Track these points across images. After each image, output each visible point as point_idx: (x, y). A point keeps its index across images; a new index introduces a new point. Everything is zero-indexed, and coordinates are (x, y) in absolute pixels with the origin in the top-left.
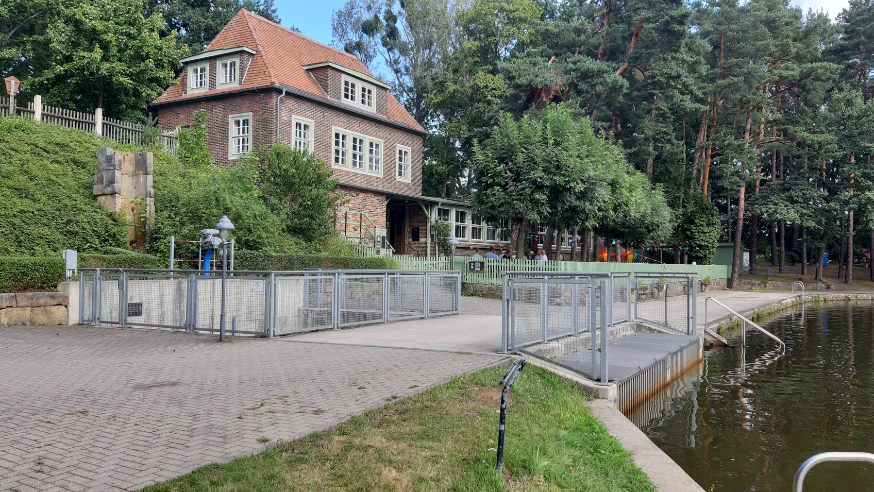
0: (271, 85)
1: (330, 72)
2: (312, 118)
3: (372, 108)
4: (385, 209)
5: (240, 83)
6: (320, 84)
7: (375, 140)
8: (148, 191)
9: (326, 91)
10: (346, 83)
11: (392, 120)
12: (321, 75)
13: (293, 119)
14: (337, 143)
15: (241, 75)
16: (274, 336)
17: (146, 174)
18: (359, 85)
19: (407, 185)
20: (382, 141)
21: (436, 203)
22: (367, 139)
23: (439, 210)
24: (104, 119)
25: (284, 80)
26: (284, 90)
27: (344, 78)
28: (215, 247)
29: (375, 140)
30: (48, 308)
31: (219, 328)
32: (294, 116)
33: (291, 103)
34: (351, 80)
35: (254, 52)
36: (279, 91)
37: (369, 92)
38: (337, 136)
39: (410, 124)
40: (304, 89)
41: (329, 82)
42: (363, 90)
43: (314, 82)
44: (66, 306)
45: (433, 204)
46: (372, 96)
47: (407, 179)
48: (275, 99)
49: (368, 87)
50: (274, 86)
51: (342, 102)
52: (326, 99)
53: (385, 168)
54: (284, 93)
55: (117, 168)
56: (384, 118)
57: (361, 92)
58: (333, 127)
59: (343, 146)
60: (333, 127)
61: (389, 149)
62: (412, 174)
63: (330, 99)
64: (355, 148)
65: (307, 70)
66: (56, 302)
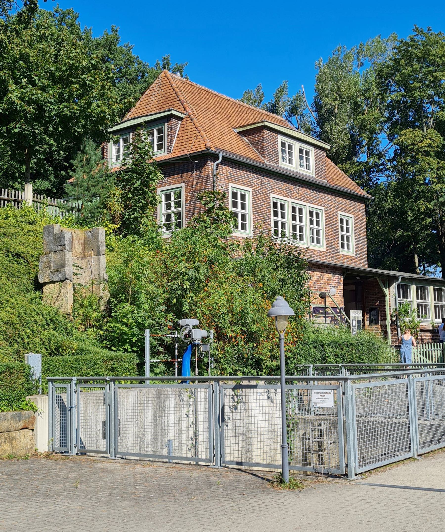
0: (207, 150)
1: (266, 132)
2: (250, 186)
3: (311, 171)
4: (342, 287)
5: (169, 151)
6: (254, 147)
7: (316, 208)
8: (101, 275)
9: (263, 154)
10: (283, 144)
11: (332, 184)
12: (256, 137)
13: (230, 188)
14: (276, 214)
15: (170, 142)
16: (356, 475)
17: (99, 254)
18: (296, 146)
19: (352, 258)
20: (323, 208)
21: (395, 278)
22: (307, 208)
23: (399, 285)
24: (34, 197)
25: (218, 145)
26: (221, 155)
27: (280, 138)
28: (197, 342)
29: (316, 208)
30: (13, 434)
31: (280, 463)
32: (231, 185)
33: (226, 170)
34: (288, 141)
35: (183, 116)
36: (215, 157)
37: (307, 153)
38: (275, 205)
39: (351, 188)
40: (239, 153)
41: (265, 144)
42: (301, 151)
43: (247, 146)
44: (33, 430)
45: (390, 280)
46: (311, 157)
47: (351, 252)
48: (211, 166)
49: (306, 147)
50: (210, 151)
51: (280, 165)
52: (264, 163)
53: (327, 241)
54: (221, 159)
55: (67, 248)
56: (323, 181)
57: (298, 154)
58: (272, 195)
59: (282, 217)
60: (272, 195)
61: (331, 217)
62: (356, 245)
63: (267, 162)
64: (294, 218)
65: (238, 133)
66: (21, 425)
